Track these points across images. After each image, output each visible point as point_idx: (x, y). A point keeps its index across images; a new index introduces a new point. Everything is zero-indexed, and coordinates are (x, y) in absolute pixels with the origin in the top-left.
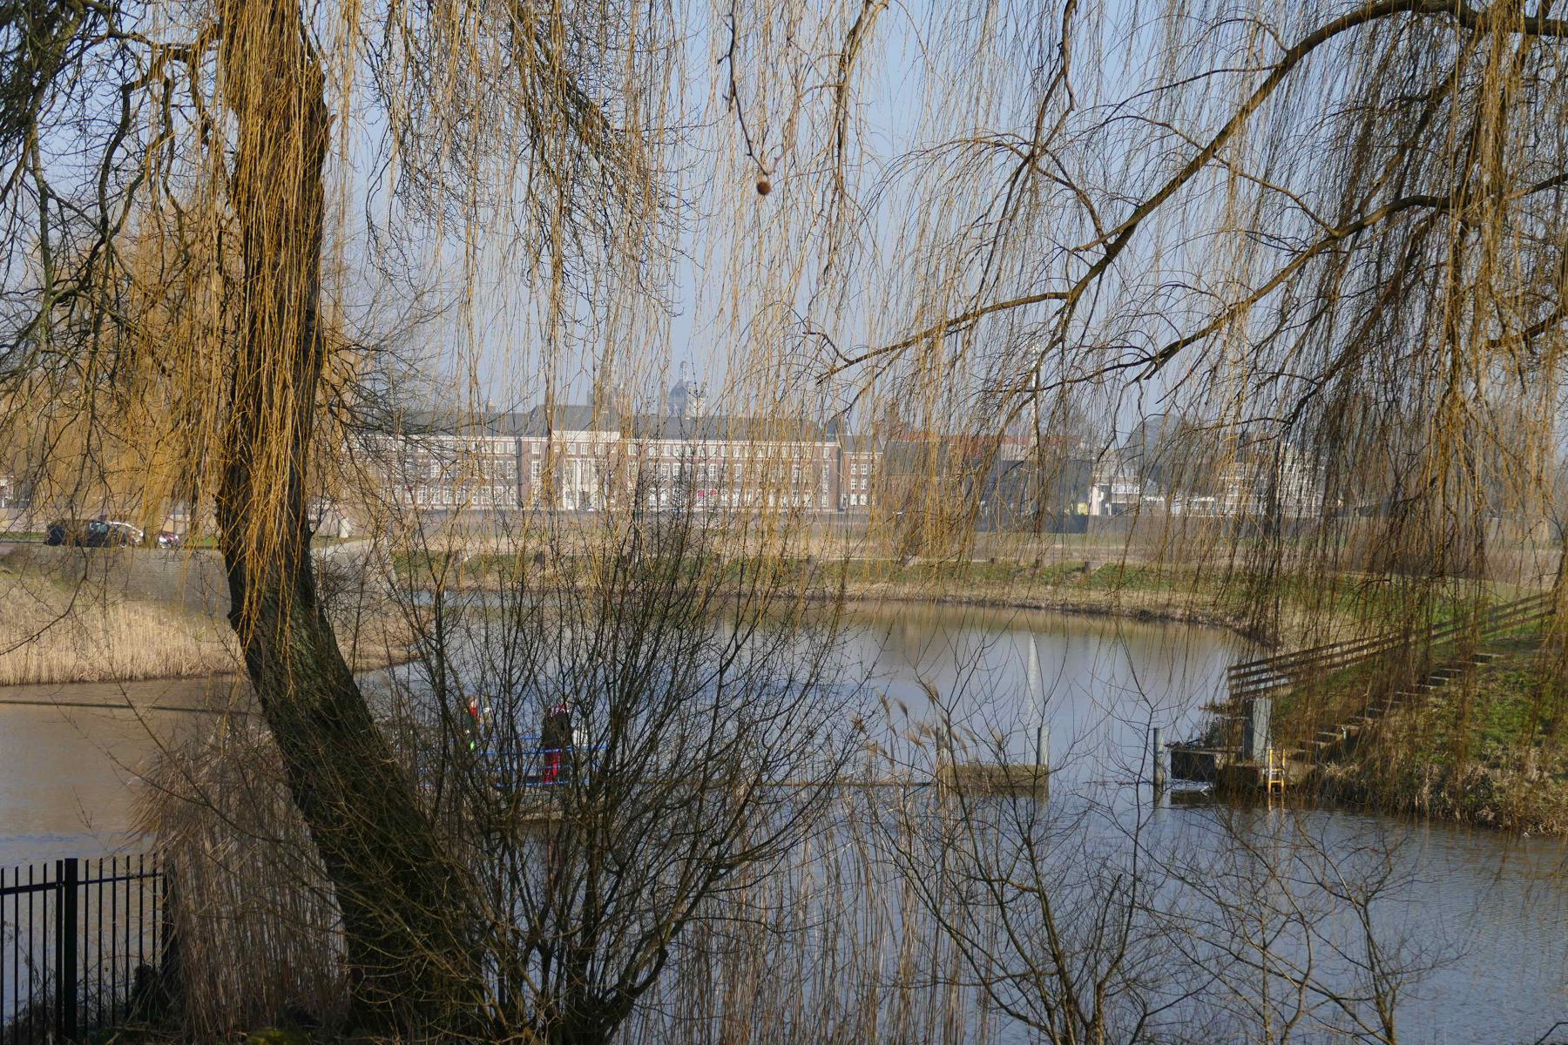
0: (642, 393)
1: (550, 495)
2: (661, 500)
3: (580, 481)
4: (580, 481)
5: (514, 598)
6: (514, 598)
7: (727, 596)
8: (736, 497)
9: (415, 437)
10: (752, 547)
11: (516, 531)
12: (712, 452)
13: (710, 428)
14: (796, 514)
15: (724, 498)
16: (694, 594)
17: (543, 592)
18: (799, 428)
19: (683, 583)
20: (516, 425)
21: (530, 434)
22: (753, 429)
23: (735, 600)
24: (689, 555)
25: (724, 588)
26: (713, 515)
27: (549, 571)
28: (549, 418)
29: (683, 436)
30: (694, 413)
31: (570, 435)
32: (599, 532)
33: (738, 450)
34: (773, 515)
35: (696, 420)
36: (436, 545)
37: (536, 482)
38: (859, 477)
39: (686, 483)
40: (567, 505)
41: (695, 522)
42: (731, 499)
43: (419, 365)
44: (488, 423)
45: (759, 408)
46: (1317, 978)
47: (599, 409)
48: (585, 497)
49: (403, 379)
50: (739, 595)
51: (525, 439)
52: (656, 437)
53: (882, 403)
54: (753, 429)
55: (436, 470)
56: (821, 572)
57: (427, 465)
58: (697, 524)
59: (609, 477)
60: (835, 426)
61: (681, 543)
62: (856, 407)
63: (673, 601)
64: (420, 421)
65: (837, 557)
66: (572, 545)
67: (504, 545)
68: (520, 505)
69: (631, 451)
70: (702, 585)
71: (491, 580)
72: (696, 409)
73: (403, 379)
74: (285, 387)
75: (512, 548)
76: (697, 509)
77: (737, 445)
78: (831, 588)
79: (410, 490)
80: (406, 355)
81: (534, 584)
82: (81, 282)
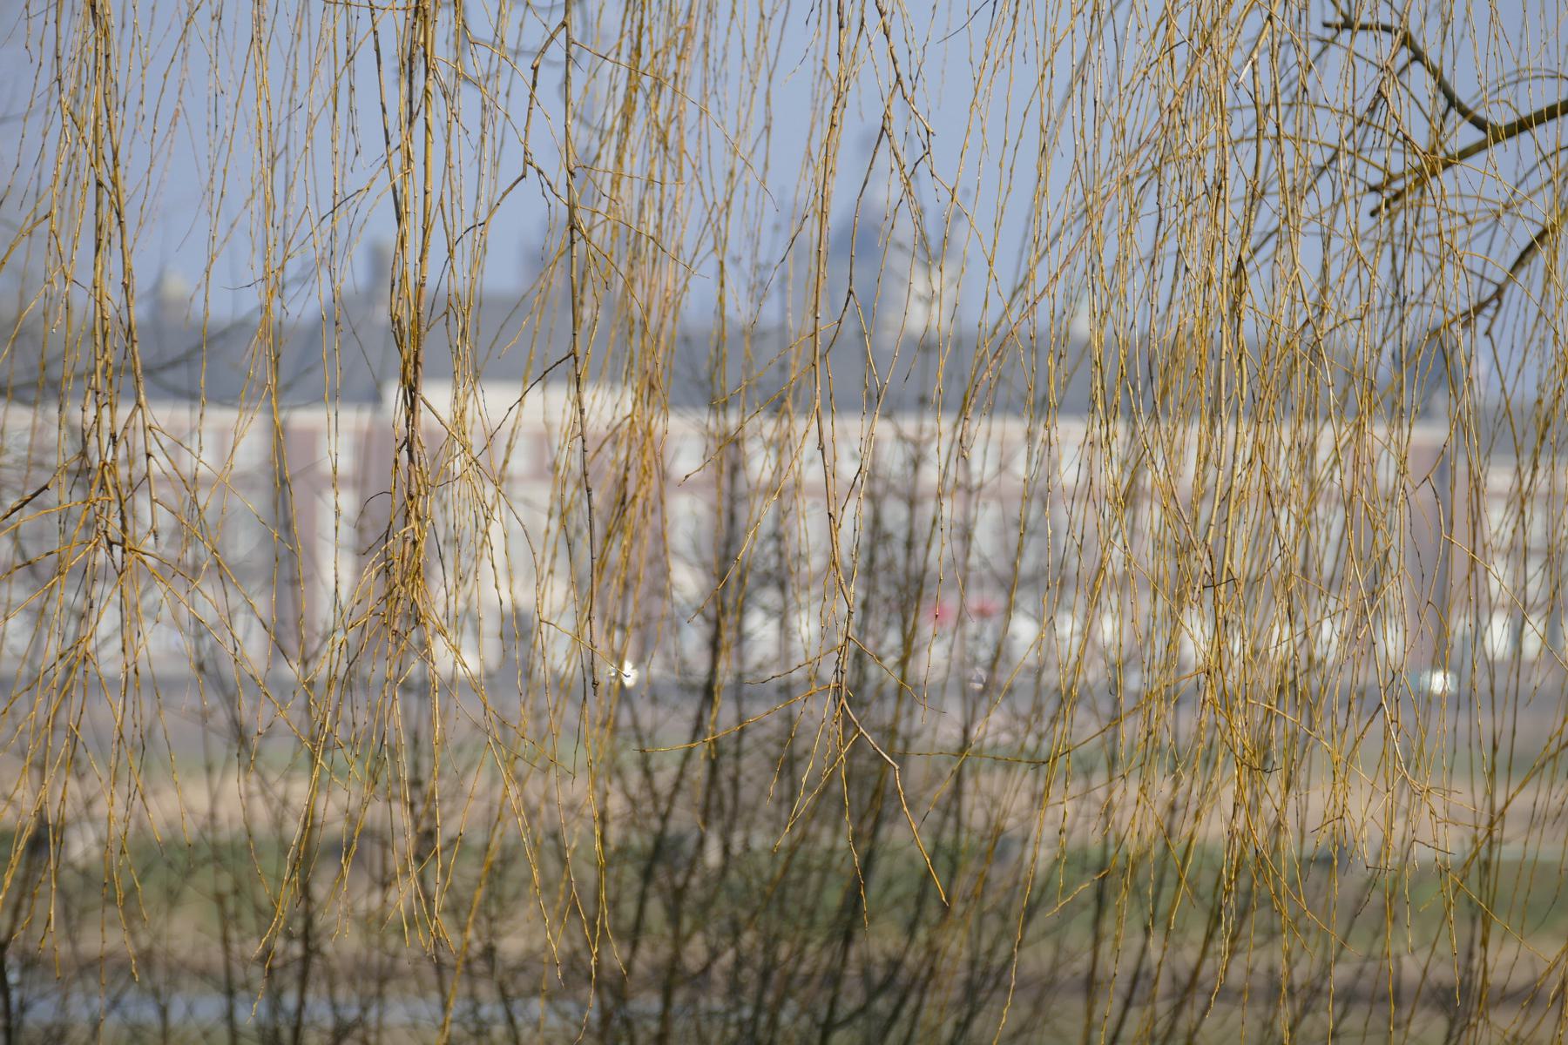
1: (397, 610)
3: (506, 574)
4: (506, 574)
5: (275, 997)
6: (275, 997)
7: (1044, 989)
8: (1068, 626)
11: (279, 751)
12: (982, 466)
14: (1297, 689)
15: (1024, 629)
16: (927, 978)
17: (379, 977)
18: (1292, 377)
19: (881, 939)
20: (278, 363)
21: (315, 399)
22: (1143, 385)
23: (1077, 1004)
24: (908, 838)
25: (1035, 958)
26: (976, 699)
27: (402, 896)
28: (414, 338)
29: (877, 401)
30: (917, 319)
31: (495, 400)
35: (926, 347)
38: (1519, 552)
39: (897, 584)
40: (462, 657)
41: (921, 717)
44: (182, 361)
45: (1156, 306)
47: (584, 309)
48: (519, 629)
50: (1091, 985)
51: (303, 418)
52: (777, 408)
54: (1143, 385)
56: (1385, 899)
58: (940, 727)
60: (1435, 365)
61: (870, 795)
62: (1513, 295)
63: (848, 1004)
65: (1455, 843)
66: (473, 801)
70: (956, 945)
71: (187, 931)
72: (918, 307)
74: (311, 121)
75: (261, 810)
76: (934, 658)
77: (1070, 433)
78: (1416, 957)
81: (344, 940)
82: (42, 839)
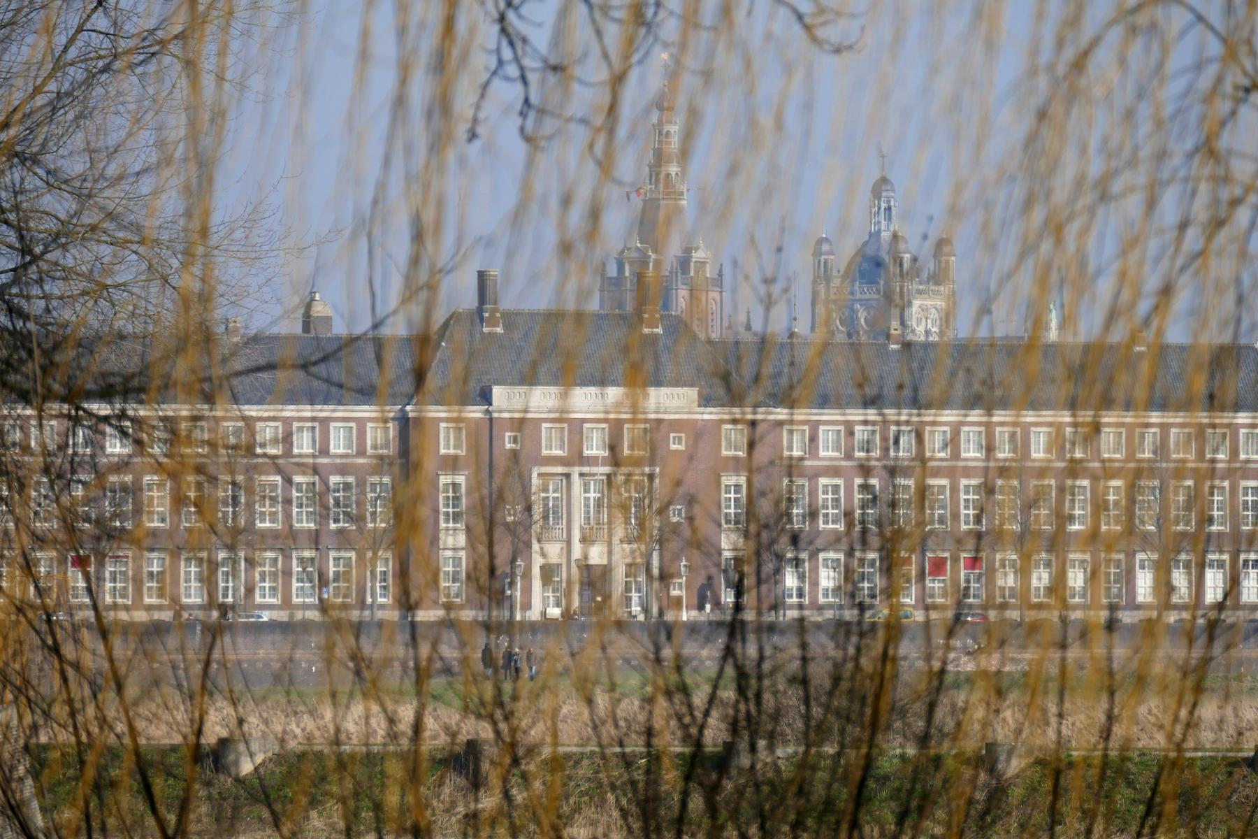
0: (757, 261)
1: (491, 582)
2: (815, 585)
4: (577, 537)
9: (101, 409)
10: (1078, 728)
11: (393, 678)
13: (984, 373)
24: (897, 749)
32: (634, 681)
33: (1041, 432)
34: (1149, 629)
36: (163, 728)
37: (453, 545)
39: (885, 536)
40: (540, 604)
42: (1017, 579)
43: (110, 197)
46: (504, 405)
49: (62, 236)
53: (800, 263)
55: (158, 498)
57: (134, 490)
59: (670, 532)
64: (111, 360)
67: (361, 723)
68: (407, 604)
69: (732, 444)
73: (62, 236)
75: (379, 725)
79: (81, 562)
80: (76, 167)
